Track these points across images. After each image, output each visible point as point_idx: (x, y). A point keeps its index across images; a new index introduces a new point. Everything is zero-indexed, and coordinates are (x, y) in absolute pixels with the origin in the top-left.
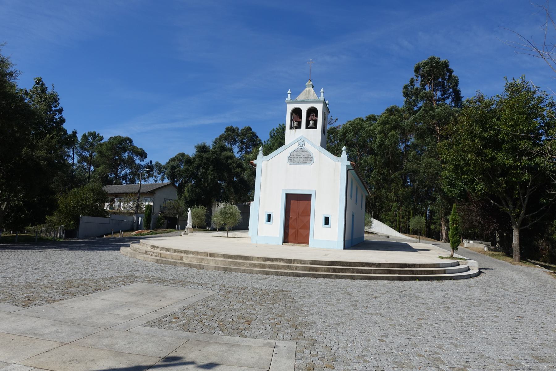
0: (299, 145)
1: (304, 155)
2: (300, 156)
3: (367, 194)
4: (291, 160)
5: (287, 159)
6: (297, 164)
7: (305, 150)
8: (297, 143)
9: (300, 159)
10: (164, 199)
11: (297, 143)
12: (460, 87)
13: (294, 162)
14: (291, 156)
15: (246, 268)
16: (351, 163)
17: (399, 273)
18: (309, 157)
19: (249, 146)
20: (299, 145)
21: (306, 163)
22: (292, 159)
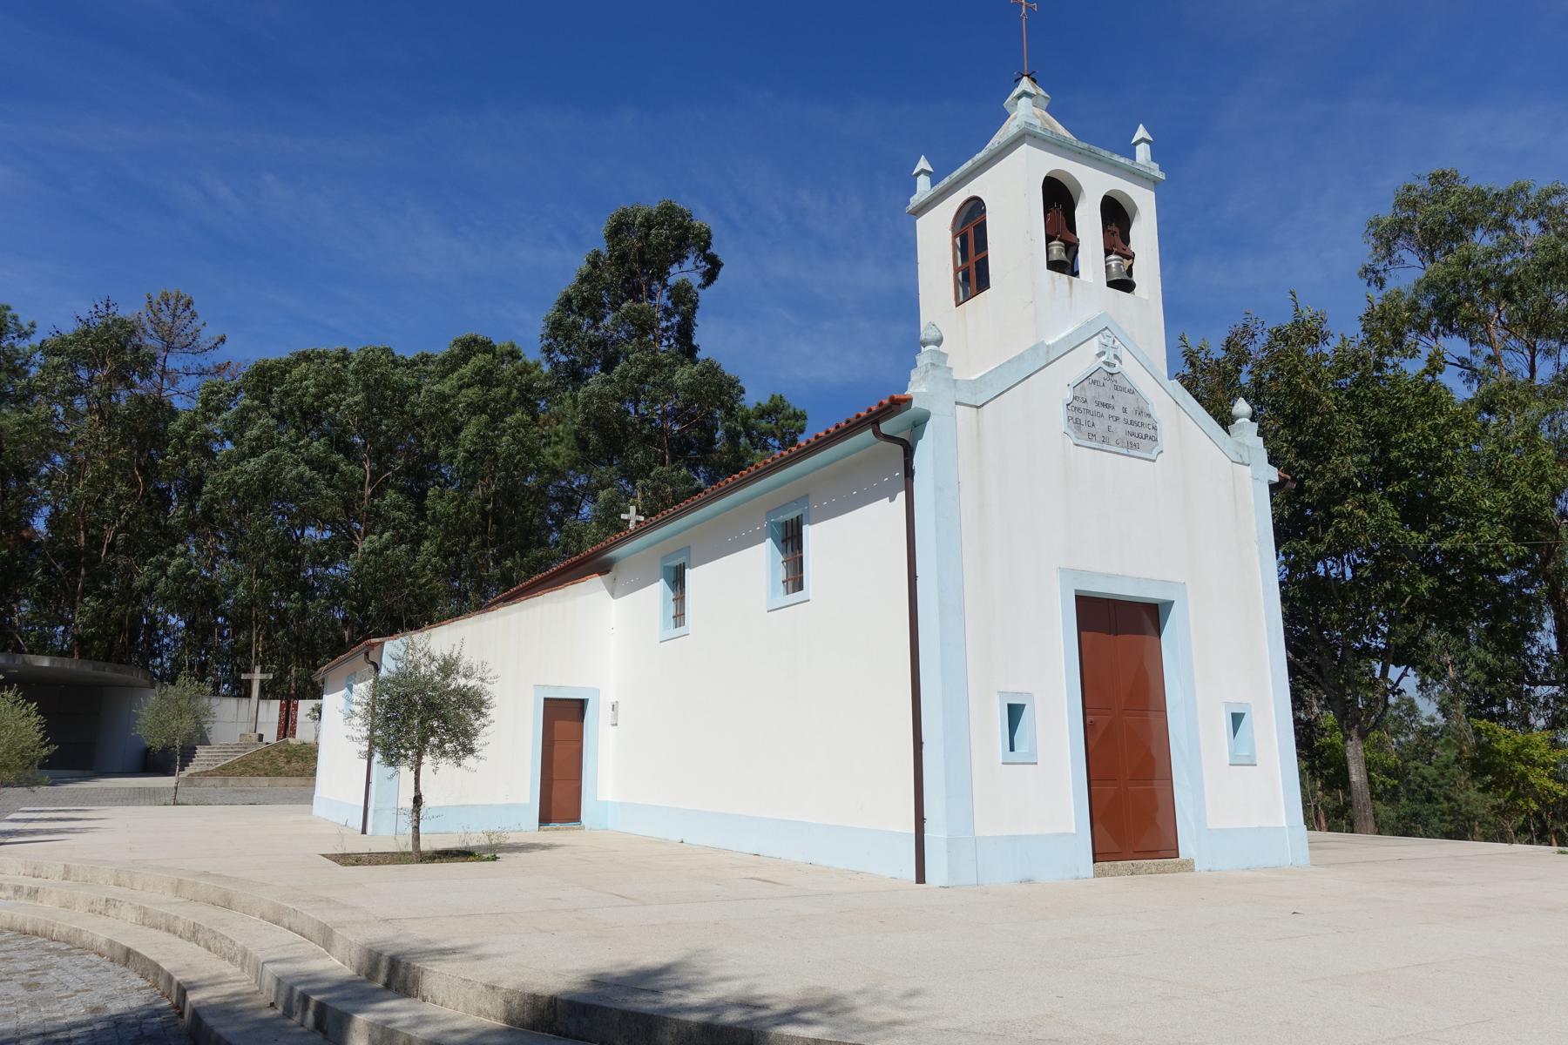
0: (1099, 355)
1: (1125, 411)
2: (1111, 412)
3: (814, 429)
4: (1077, 422)
5: (1061, 414)
6: (1105, 447)
7: (1128, 387)
8: (1094, 346)
9: (1114, 425)
10: (1107, 328)
11: (1094, 346)
12: (698, 318)
13: (1092, 436)
14: (1076, 403)
15: (185, 879)
16: (1282, 475)
17: (1447, 827)
18: (1146, 420)
19: (86, 592)
20: (1099, 355)
21: (1135, 446)
22: (1083, 417)
